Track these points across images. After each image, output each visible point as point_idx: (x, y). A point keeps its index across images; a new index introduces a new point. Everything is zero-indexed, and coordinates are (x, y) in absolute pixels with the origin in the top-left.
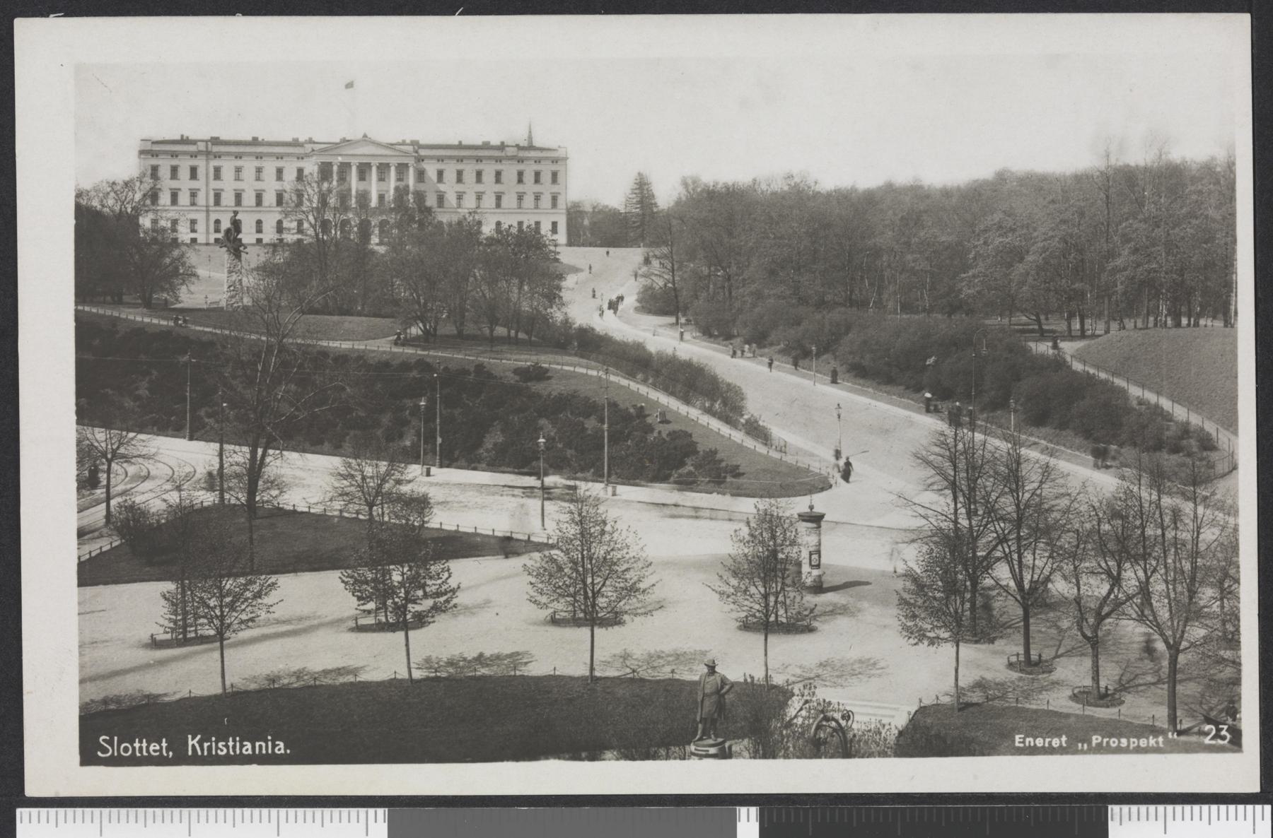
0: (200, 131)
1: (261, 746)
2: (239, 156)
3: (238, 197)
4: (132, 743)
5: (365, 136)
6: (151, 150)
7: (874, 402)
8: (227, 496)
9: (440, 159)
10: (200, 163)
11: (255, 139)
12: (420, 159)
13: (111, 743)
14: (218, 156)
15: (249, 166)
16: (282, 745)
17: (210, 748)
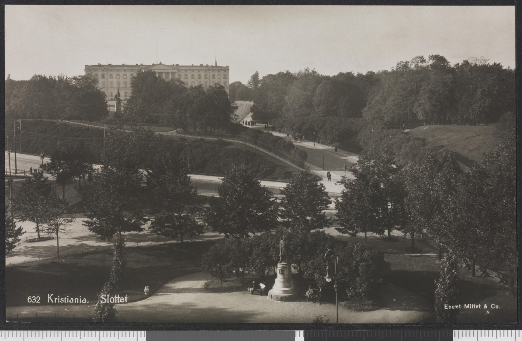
0: (104, 63)
1: (77, 300)
2: (118, 70)
3: (118, 83)
4: (114, 297)
5: (160, 63)
6: (87, 68)
7: (444, 126)
8: (41, 234)
9: (186, 71)
10: (105, 73)
11: (123, 64)
12: (179, 71)
13: (106, 298)
14: (111, 70)
15: (122, 74)
16: (85, 299)
17: (57, 301)
